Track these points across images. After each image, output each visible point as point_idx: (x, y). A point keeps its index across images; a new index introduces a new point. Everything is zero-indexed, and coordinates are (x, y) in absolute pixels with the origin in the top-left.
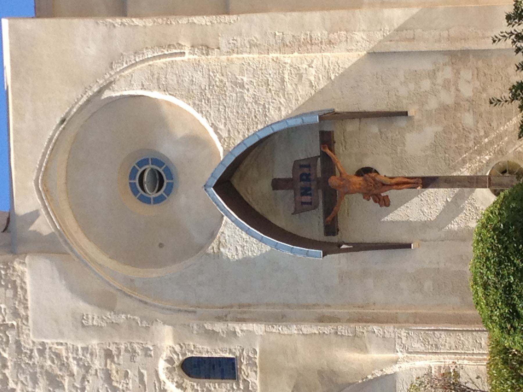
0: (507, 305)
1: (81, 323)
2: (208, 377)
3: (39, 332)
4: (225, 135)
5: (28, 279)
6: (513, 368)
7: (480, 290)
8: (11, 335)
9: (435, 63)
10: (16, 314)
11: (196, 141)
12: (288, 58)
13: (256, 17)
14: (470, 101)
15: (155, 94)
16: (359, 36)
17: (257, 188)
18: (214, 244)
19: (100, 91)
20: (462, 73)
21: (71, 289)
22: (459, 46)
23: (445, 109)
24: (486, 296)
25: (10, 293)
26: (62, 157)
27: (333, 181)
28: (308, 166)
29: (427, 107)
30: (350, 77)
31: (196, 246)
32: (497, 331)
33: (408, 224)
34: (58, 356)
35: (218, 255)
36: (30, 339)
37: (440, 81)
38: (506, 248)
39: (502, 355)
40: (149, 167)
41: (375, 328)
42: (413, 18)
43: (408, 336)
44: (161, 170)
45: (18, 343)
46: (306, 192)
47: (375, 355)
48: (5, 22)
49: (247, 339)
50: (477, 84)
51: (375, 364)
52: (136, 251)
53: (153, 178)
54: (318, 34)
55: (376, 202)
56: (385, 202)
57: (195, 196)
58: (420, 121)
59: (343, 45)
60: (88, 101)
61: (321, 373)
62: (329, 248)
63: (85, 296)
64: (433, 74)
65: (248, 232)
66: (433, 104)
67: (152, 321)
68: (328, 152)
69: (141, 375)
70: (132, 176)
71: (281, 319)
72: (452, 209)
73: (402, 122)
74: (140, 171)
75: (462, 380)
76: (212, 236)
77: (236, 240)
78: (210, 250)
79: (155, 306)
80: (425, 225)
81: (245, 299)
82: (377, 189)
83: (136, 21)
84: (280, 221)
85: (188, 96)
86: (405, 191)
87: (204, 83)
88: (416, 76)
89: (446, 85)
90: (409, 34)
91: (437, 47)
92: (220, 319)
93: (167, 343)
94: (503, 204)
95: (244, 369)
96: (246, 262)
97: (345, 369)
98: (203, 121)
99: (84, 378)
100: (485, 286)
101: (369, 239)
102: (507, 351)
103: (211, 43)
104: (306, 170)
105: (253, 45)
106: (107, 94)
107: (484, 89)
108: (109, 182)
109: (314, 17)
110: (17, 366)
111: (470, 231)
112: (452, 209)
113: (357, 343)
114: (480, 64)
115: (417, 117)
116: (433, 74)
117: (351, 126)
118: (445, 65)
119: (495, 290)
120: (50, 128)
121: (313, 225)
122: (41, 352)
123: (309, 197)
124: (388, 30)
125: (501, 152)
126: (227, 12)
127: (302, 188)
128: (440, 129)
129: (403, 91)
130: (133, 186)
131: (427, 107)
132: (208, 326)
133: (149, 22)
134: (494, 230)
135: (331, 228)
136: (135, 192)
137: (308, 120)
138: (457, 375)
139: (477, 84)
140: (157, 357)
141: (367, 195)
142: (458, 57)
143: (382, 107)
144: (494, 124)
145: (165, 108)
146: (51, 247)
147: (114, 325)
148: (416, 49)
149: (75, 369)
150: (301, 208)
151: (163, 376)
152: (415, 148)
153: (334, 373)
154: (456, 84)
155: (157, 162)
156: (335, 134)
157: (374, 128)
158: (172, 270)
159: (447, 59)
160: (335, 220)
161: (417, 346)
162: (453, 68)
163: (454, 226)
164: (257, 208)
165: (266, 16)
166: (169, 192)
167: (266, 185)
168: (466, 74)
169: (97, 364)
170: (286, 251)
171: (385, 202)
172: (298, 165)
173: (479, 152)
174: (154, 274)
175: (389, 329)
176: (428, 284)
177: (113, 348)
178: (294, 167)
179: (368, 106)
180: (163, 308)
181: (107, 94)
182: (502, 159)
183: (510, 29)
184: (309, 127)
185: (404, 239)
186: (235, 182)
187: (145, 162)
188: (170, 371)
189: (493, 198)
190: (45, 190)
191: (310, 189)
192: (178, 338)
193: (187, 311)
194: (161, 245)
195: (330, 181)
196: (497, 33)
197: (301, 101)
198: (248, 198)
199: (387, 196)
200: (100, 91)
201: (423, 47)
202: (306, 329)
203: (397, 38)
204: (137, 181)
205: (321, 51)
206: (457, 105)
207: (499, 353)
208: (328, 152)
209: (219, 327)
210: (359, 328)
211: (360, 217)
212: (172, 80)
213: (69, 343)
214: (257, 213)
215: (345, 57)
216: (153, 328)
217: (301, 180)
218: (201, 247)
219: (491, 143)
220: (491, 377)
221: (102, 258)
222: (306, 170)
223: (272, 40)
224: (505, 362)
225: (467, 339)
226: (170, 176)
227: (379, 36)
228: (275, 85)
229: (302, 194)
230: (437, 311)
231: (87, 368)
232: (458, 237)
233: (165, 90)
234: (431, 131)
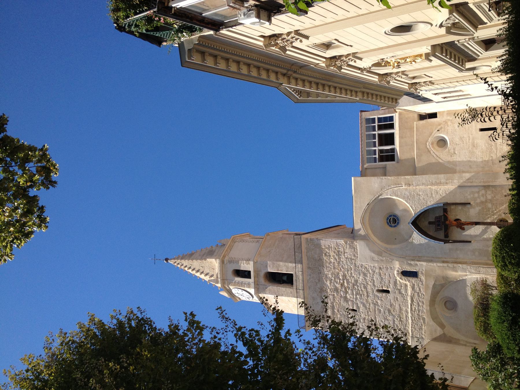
0: (503, 262)
1: (373, 259)
2: (409, 276)
3: (361, 261)
4: (414, 209)
5: (358, 247)
6: (505, 280)
7: (494, 257)
8: (353, 261)
10: (354, 256)
11: (406, 211)
12: (434, 188)
13: (424, 176)
14: (491, 200)
15: (394, 197)
16: (455, 181)
17: (424, 224)
18: (411, 239)
19: (379, 196)
21: (370, 250)
22: (486, 184)
23: (482, 202)
24: (496, 259)
25: (353, 250)
26: (368, 215)
27: (447, 222)
30: (452, 193)
31: (406, 239)
32: (500, 270)
33: (471, 236)
34: (366, 268)
35: (412, 242)
36: (358, 263)
38: (503, 245)
39: (501, 276)
40: (392, 217)
41: (460, 265)
42: (472, 176)
43: (470, 268)
45: (355, 264)
46: (438, 225)
47: (460, 273)
48: (353, 178)
49: (421, 266)
50: (493, 195)
51: (460, 276)
52: (388, 240)
53: (393, 220)
54: (443, 181)
56: (463, 229)
57: (406, 226)
59: (450, 184)
60: (375, 199)
61: (443, 278)
62: (446, 242)
63: (374, 252)
64: (478, 192)
65: (421, 236)
66: (478, 201)
67: (393, 260)
69: (390, 275)
70: (387, 219)
71: (431, 261)
72: (484, 232)
73: (468, 206)
75: (488, 283)
76: (411, 237)
77: (417, 238)
78: (410, 241)
80: (476, 236)
81: (420, 255)
82: (461, 225)
83: (389, 178)
85: (404, 198)
86: (470, 226)
87: (408, 194)
89: (483, 195)
90: (471, 181)
91: (480, 184)
92: (413, 260)
93: (397, 266)
94: (502, 232)
95: (420, 275)
96: (420, 245)
97: (451, 277)
98: (408, 205)
99: (373, 275)
100: (496, 256)
101: (458, 239)
102: (502, 275)
103: (411, 183)
105: (423, 184)
106: (380, 197)
108: (381, 221)
109: (442, 176)
110: (355, 270)
111: (490, 239)
112: (484, 232)
113: (454, 269)
114: (493, 189)
115: (474, 204)
116: (478, 192)
117: (453, 207)
119: (317, 281)
120: (364, 206)
121: (441, 235)
122: (362, 267)
124: (464, 179)
125: (500, 215)
126: (415, 175)
128: (480, 208)
129: (469, 197)
130: (387, 222)
132: (409, 262)
133: (393, 178)
134: (499, 240)
135: (447, 236)
136: (388, 224)
137: (439, 205)
138: (486, 281)
139: (493, 195)
140: (394, 270)
141: (458, 227)
142: (486, 187)
143: (463, 202)
144: (498, 207)
145: (397, 201)
146: (364, 238)
147: (382, 260)
149: (371, 272)
150: (437, 230)
151: (396, 275)
152: (473, 214)
153: (447, 278)
154: (486, 195)
155: (394, 216)
157: (460, 207)
160: (447, 234)
161: (473, 271)
163: (485, 237)
165: (427, 176)
166: (398, 224)
167: (426, 223)
168: (489, 192)
169: (377, 271)
170: (433, 242)
171: (463, 229)
172: (436, 218)
173: (493, 215)
174: (394, 247)
175: (465, 266)
176: (477, 253)
177: (382, 267)
179: (458, 201)
181: (380, 197)
182: (500, 217)
183: (510, 192)
184: (440, 207)
185: (469, 240)
186: (417, 222)
187: (390, 216)
188: (398, 274)
189: (498, 230)
190: (363, 223)
192: (400, 265)
193: (402, 258)
196: (505, 194)
197: (437, 200)
198: (421, 227)
200: (379, 196)
201: (475, 184)
202: (439, 264)
205: (444, 185)
206: (486, 201)
207: (500, 275)
209: (412, 263)
210: (455, 265)
211: (456, 233)
212: (399, 193)
213: (369, 264)
215: (451, 187)
216: (393, 262)
218: (407, 240)
219: (497, 212)
220: (498, 283)
223: (429, 183)
224: (502, 279)
225: (489, 270)
226: (398, 220)
227: (462, 181)
228: (429, 195)
230: (480, 261)
231: (374, 272)
232: (487, 240)
233: (397, 196)
234: (478, 209)
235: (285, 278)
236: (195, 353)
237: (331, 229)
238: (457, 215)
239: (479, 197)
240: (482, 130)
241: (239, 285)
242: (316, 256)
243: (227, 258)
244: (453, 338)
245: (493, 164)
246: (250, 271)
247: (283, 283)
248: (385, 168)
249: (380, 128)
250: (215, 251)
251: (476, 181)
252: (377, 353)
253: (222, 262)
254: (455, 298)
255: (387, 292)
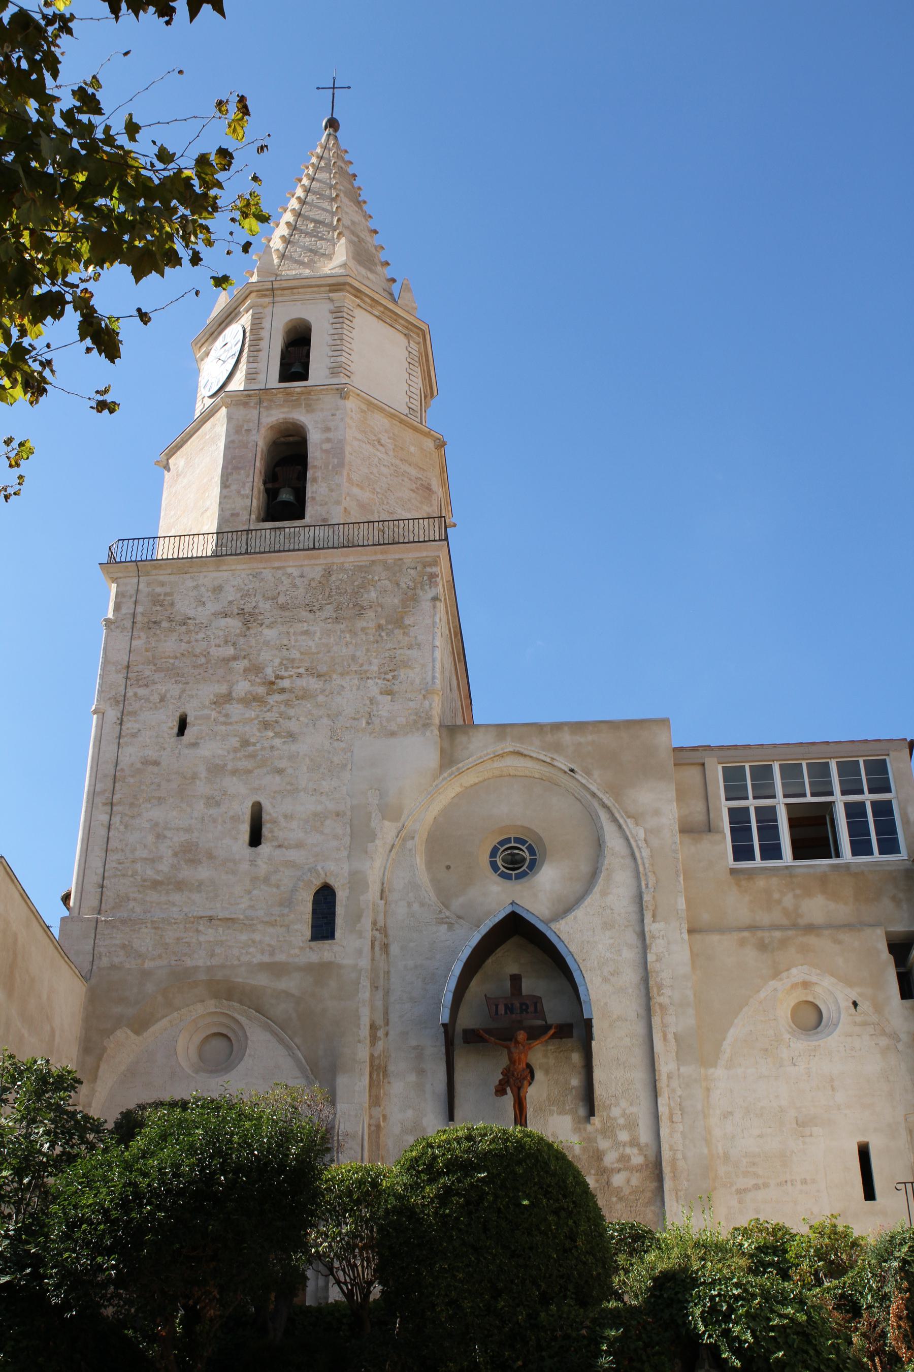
9: (647, 1145)
14: (608, 1183)
20: (638, 1174)
22: (667, 1170)
28: (536, 1011)
29: (599, 1138)
37: (628, 1150)
40: (526, 855)
44: (524, 868)
46: (509, 1009)
50: (626, 1191)
55: (500, 1081)
57: (495, 898)
58: (585, 1130)
64: (634, 1143)
68: (552, 1032)
70: (517, 840)
73: (582, 1112)
74: (523, 848)
79: (387, 860)
84: (475, 986)
88: (631, 1125)
89: (624, 1159)
104: (531, 1009)
107: (620, 1199)
114: (648, 1194)
116: (634, 1143)
117: (576, 1058)
118: (645, 1156)
119: (281, 600)
123: (503, 1012)
127: (512, 1005)
130: (508, 840)
131: (599, 1138)
135: (473, 1038)
142: (656, 1170)
148: (662, 1124)
155: (533, 865)
156: (569, 1040)
157: (575, 1082)
158: (423, 877)
159: (652, 1158)
162: (642, 1165)
164: (490, 961)
166: (503, 876)
167: (514, 969)
168: (636, 1180)
174: (420, 861)
178: (534, 996)
179: (598, 1075)
180: (385, 868)
191: (512, 1013)
194: (448, 867)
195: (522, 1032)
198: (499, 952)
199: (572, 1037)
203: (672, 1104)
204: (513, 844)
208: (552, 1032)
214: (484, 962)
217: (521, 1004)
221: (436, 808)
222: (531, 1009)
229: (506, 1006)
235: (286, 496)
236: (324, 1290)
237: (460, 666)
238: (547, 1072)
239: (617, 1144)
240: (864, 1154)
241: (253, 341)
242: (373, 595)
243: (348, 300)
244: (100, 1058)
245: (739, 1192)
246: (305, 378)
247: (267, 491)
248: (709, 828)
249: (855, 811)
250: (371, 271)
251: (678, 1136)
252: (633, 1281)
253: (337, 286)
254: (241, 1067)
255: (256, 839)
